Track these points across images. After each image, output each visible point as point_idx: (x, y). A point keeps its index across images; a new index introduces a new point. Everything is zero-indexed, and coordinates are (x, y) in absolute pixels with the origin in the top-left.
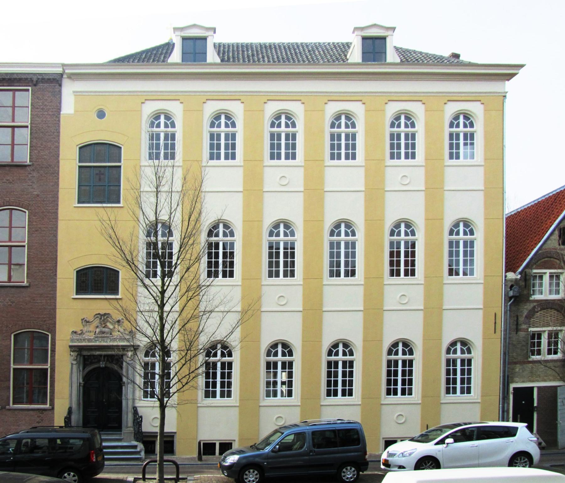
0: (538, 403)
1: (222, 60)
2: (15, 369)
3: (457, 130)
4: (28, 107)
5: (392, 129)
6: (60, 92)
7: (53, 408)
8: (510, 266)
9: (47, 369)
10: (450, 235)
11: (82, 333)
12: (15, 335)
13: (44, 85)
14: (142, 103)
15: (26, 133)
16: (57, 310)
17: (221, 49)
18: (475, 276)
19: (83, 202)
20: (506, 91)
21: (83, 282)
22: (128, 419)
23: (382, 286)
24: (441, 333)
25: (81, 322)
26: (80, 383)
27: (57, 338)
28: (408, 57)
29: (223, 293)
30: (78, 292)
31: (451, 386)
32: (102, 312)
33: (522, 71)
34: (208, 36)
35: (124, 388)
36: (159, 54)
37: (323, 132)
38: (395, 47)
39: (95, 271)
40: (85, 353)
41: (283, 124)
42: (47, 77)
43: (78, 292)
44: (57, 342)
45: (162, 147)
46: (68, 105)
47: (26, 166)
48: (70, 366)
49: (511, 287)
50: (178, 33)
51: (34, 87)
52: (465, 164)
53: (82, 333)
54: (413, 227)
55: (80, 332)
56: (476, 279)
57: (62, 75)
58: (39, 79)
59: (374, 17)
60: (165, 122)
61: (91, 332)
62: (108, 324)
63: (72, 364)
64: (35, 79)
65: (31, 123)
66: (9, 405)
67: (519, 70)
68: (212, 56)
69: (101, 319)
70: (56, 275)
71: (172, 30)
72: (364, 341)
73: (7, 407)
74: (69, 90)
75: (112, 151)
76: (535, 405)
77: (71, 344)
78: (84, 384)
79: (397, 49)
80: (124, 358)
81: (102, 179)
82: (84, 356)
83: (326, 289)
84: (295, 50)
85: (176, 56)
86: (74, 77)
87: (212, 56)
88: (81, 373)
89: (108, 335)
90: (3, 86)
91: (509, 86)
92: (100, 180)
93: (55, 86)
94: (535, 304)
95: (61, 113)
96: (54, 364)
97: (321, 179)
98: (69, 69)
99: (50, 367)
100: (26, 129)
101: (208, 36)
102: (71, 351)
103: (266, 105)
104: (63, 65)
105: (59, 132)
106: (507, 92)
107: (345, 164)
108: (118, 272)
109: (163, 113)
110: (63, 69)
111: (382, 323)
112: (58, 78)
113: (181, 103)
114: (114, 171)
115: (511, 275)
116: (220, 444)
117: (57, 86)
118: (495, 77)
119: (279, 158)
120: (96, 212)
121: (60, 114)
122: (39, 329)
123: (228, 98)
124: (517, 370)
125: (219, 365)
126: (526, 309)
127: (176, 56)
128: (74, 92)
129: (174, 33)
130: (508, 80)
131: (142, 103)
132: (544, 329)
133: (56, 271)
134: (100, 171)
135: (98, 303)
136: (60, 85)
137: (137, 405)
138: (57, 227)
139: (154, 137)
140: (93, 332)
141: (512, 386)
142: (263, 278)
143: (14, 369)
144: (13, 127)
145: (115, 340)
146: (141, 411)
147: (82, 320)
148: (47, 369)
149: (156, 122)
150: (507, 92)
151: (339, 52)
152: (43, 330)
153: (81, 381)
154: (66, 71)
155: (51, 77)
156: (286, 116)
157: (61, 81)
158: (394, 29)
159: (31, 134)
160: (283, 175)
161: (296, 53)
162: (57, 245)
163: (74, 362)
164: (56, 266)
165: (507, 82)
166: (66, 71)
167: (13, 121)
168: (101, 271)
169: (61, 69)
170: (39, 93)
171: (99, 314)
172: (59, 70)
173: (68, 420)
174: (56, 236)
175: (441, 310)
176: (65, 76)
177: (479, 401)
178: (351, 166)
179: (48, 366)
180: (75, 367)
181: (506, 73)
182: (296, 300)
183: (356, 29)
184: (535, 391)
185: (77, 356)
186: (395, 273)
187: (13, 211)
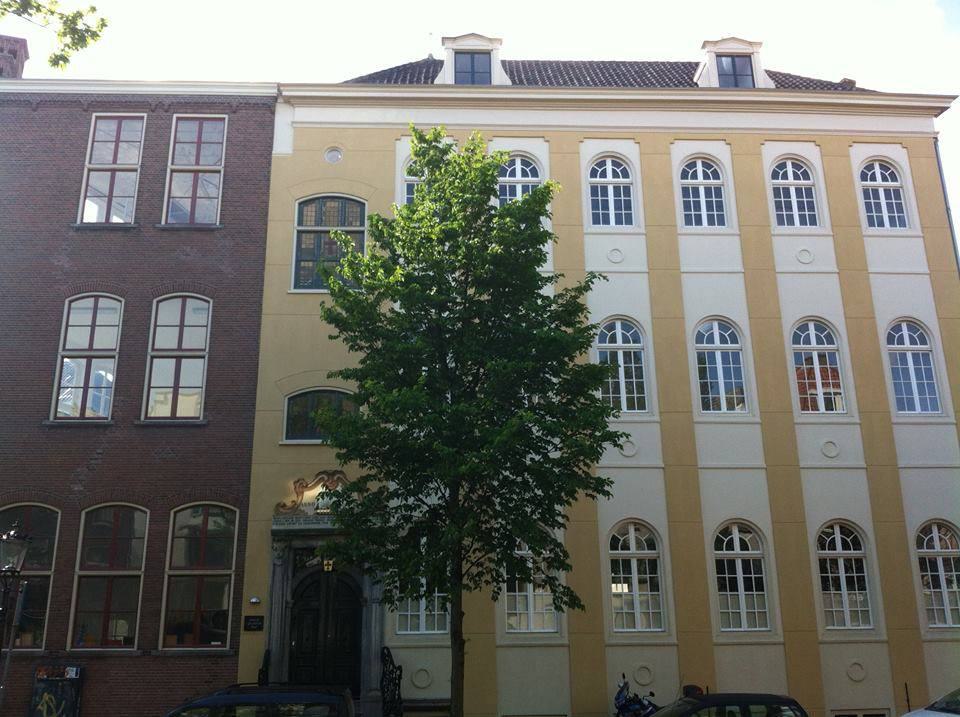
1: (514, 82)
2: (81, 577)
4: (222, 143)
5: (594, 180)
6: (272, 122)
7: (237, 653)
12: (87, 513)
13: (251, 116)
15: (218, 179)
17: (510, 68)
19: (300, 287)
20: (936, 130)
22: (373, 672)
26: (287, 603)
27: (250, 518)
28: (784, 82)
33: (954, 105)
35: (364, 609)
36: (421, 72)
37: (670, 183)
38: (766, 71)
40: (298, 543)
41: (519, 172)
46: (283, 142)
47: (213, 230)
50: (449, 44)
51: (232, 115)
52: (801, 232)
54: (636, 328)
57: (275, 99)
59: (735, 25)
60: (522, 169)
63: (274, 565)
65: (225, 166)
66: (156, 648)
67: (950, 102)
68: (499, 76)
70: (254, 405)
71: (440, 40)
72: (874, 521)
73: (154, 652)
74: (285, 121)
77: (274, 527)
78: (294, 604)
79: (504, 63)
82: (296, 549)
84: (540, 72)
85: (446, 76)
86: (289, 101)
87: (499, 76)
88: (290, 582)
90: (186, 113)
91: (941, 124)
95: (274, 152)
96: (243, 567)
97: (674, 251)
98: (287, 91)
99: (236, 571)
100: (217, 175)
102: (274, 540)
103: (672, 146)
104: (279, 86)
106: (938, 133)
110: (279, 90)
111: (697, 489)
119: (606, 221)
121: (271, 153)
122: (221, 502)
123: (794, 138)
125: (841, 563)
127: (446, 76)
129: (443, 44)
130: (936, 116)
131: (397, 140)
136: (273, 113)
137: (388, 643)
139: (870, 194)
142: (795, 414)
143: (80, 577)
144: (113, 171)
146: (399, 657)
150: (938, 133)
151: (680, 75)
152: (227, 503)
153: (289, 598)
154: (284, 93)
156: (613, 161)
157: (275, 106)
159: (224, 182)
160: (805, 248)
161: (617, 74)
163: (279, 563)
165: (934, 119)
166: (284, 93)
167: (197, 163)
169: (276, 91)
172: (274, 92)
173: (264, 674)
175: (895, 469)
176: (280, 100)
179: (232, 572)
180: (278, 569)
181: (935, 107)
183: (705, 44)
185: (283, 550)
187: (188, 300)
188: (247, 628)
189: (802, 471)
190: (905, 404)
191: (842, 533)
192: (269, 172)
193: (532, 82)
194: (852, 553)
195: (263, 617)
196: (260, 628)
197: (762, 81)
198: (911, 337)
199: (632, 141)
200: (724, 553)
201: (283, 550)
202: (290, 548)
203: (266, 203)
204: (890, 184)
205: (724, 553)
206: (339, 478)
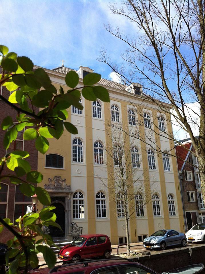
8: (179, 169)
9: (6, 204)
10: (73, 143)
11: (49, 186)
18: (83, 162)
23: (70, 165)
24: (166, 190)
25: (48, 180)
29: (101, 171)
30: (46, 166)
31: (75, 214)
43: (46, 166)
49: (181, 175)
53: (49, 186)
55: (48, 185)
56: (171, 172)
61: (52, 185)
62: (60, 181)
69: (57, 179)
70: (37, 157)
80: (66, 198)
83: (72, 166)
89: (60, 187)
94: (187, 182)
107: (97, 119)
108: (63, 158)
109: (115, 105)
115: (180, 172)
116: (144, 236)
124: (186, 206)
126: (185, 183)
132: (190, 191)
133: (37, 155)
135: (54, 171)
140: (53, 185)
145: (63, 189)
147: (49, 179)
148: (6, 204)
171: (56, 176)
177: (179, 217)
189: (72, 177)
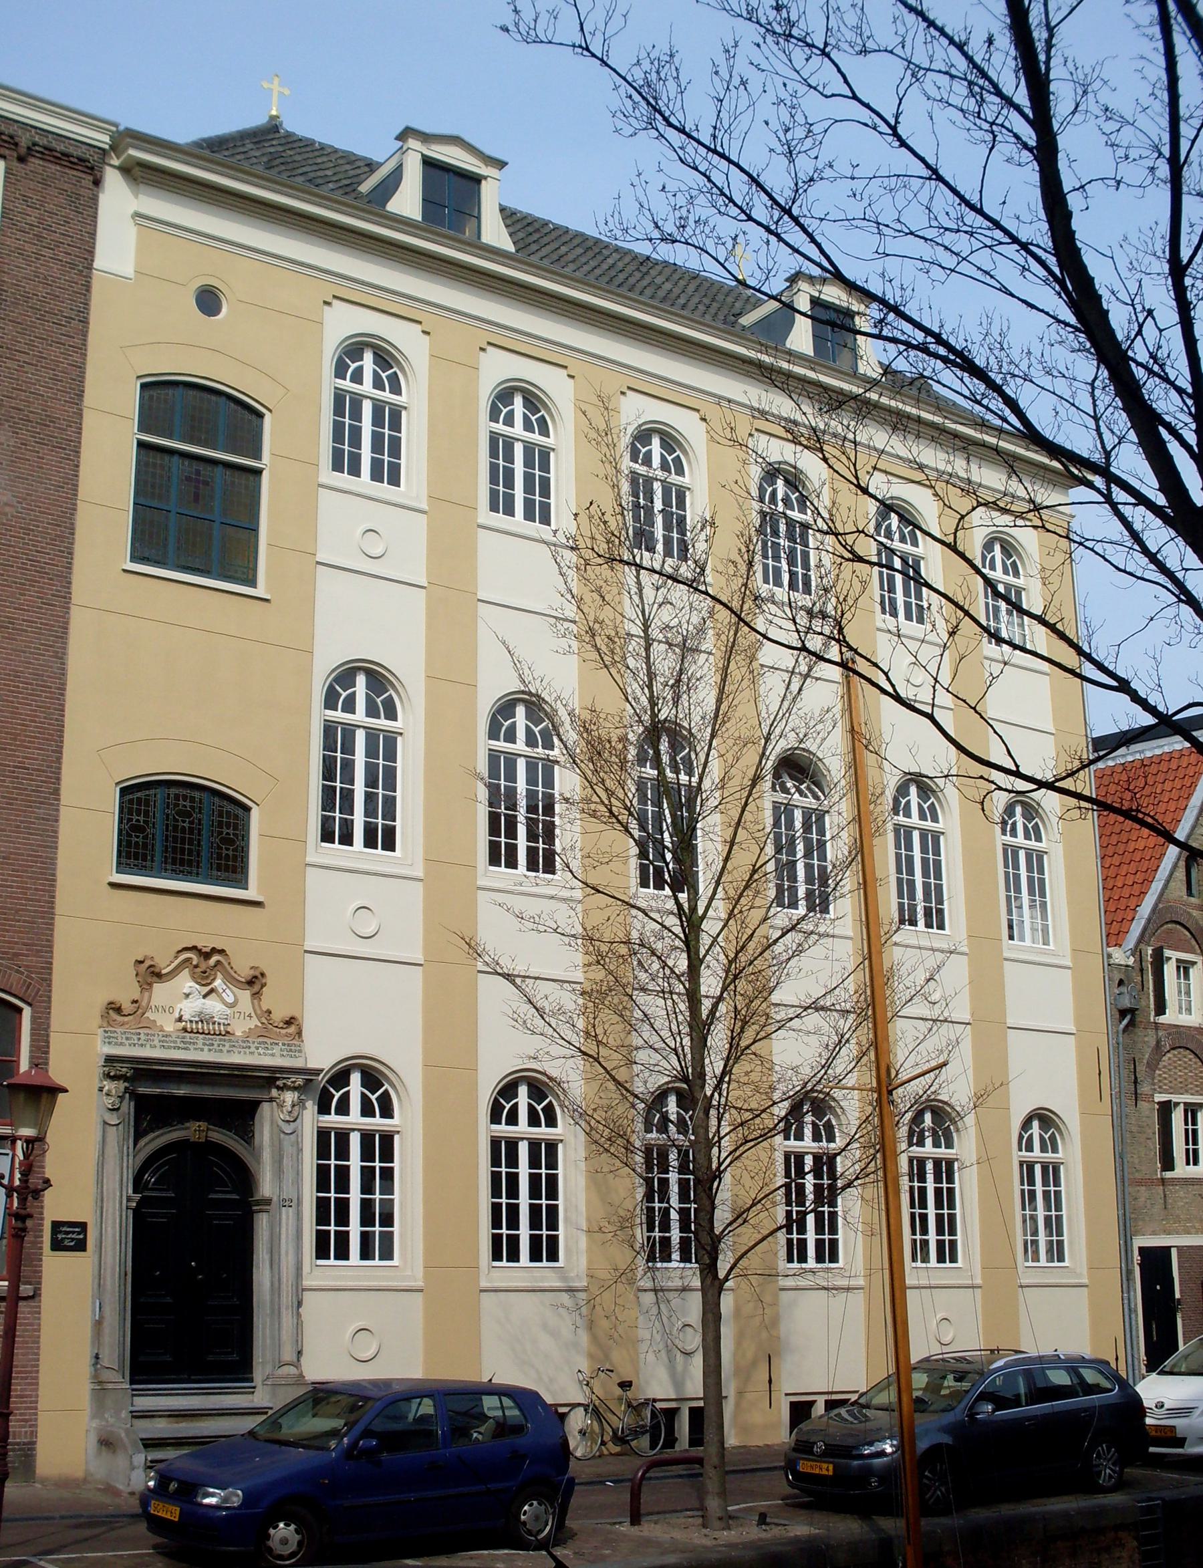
0: (1181, 1291)
3: (354, 387)
6: (94, 202)
14: (326, 303)
16: (58, 921)
21: (137, 828)
32: (206, 944)
34: (485, 178)
39: (177, 797)
42: (61, 147)
44: (54, 1039)
45: (366, 441)
48: (100, 1133)
58: (35, 144)
64: (24, 140)
70: (57, 792)
75: (238, 418)
76: (1178, 1296)
79: (509, 215)
81: (202, 499)
86: (140, 175)
92: (197, 498)
93: (79, 180)
101: (485, 178)
105: (85, 322)
112: (93, 158)
113: (569, 376)
114: (241, 479)
117: (87, 180)
118: (738, 364)
120: (183, 601)
121: (90, 267)
128: (137, 215)
134: (198, 473)
135: (178, 912)
136: (97, 183)
138: (65, 627)
141: (1140, 1242)
149: (353, 366)
155: (71, 150)
158: (501, 164)
162: (62, 688)
164: (59, 760)
168: (192, 800)
170: (32, 185)
171: (194, 948)
174: (61, 657)
178: (498, 531)
182: (405, 932)
184: (1174, 1252)
186: (501, 855)
188: (57, 1246)
190: (1011, 938)
191: (364, 1084)
192: (87, 305)
193: (555, 267)
194: (377, 1122)
195: (83, 1226)
196: (81, 1246)
197: (494, 232)
198: (529, 731)
199: (696, 415)
200: (503, 1129)
201: (122, 1098)
202: (135, 1096)
203: (81, 368)
204: (536, 437)
205: (503, 1129)
206: (218, 962)
